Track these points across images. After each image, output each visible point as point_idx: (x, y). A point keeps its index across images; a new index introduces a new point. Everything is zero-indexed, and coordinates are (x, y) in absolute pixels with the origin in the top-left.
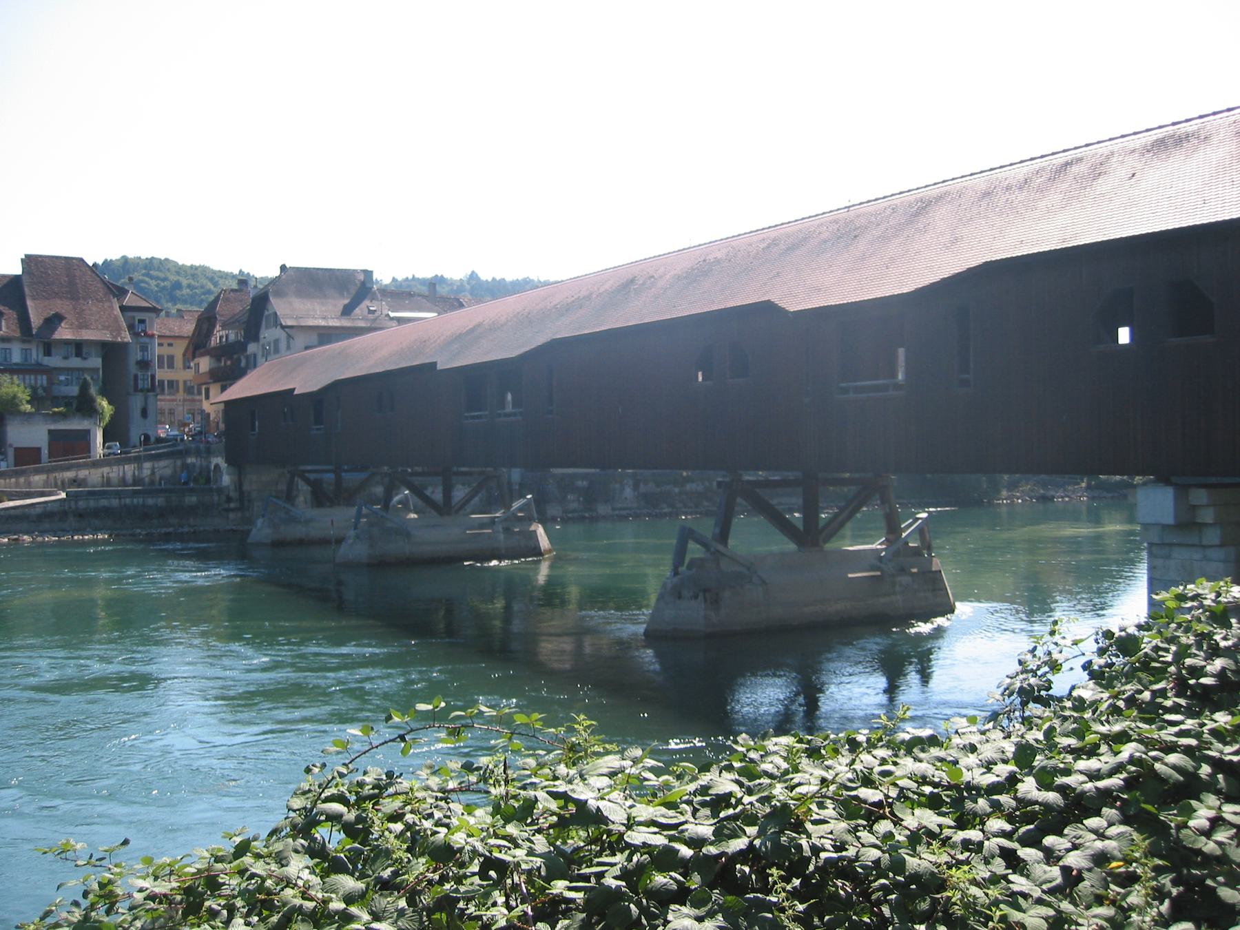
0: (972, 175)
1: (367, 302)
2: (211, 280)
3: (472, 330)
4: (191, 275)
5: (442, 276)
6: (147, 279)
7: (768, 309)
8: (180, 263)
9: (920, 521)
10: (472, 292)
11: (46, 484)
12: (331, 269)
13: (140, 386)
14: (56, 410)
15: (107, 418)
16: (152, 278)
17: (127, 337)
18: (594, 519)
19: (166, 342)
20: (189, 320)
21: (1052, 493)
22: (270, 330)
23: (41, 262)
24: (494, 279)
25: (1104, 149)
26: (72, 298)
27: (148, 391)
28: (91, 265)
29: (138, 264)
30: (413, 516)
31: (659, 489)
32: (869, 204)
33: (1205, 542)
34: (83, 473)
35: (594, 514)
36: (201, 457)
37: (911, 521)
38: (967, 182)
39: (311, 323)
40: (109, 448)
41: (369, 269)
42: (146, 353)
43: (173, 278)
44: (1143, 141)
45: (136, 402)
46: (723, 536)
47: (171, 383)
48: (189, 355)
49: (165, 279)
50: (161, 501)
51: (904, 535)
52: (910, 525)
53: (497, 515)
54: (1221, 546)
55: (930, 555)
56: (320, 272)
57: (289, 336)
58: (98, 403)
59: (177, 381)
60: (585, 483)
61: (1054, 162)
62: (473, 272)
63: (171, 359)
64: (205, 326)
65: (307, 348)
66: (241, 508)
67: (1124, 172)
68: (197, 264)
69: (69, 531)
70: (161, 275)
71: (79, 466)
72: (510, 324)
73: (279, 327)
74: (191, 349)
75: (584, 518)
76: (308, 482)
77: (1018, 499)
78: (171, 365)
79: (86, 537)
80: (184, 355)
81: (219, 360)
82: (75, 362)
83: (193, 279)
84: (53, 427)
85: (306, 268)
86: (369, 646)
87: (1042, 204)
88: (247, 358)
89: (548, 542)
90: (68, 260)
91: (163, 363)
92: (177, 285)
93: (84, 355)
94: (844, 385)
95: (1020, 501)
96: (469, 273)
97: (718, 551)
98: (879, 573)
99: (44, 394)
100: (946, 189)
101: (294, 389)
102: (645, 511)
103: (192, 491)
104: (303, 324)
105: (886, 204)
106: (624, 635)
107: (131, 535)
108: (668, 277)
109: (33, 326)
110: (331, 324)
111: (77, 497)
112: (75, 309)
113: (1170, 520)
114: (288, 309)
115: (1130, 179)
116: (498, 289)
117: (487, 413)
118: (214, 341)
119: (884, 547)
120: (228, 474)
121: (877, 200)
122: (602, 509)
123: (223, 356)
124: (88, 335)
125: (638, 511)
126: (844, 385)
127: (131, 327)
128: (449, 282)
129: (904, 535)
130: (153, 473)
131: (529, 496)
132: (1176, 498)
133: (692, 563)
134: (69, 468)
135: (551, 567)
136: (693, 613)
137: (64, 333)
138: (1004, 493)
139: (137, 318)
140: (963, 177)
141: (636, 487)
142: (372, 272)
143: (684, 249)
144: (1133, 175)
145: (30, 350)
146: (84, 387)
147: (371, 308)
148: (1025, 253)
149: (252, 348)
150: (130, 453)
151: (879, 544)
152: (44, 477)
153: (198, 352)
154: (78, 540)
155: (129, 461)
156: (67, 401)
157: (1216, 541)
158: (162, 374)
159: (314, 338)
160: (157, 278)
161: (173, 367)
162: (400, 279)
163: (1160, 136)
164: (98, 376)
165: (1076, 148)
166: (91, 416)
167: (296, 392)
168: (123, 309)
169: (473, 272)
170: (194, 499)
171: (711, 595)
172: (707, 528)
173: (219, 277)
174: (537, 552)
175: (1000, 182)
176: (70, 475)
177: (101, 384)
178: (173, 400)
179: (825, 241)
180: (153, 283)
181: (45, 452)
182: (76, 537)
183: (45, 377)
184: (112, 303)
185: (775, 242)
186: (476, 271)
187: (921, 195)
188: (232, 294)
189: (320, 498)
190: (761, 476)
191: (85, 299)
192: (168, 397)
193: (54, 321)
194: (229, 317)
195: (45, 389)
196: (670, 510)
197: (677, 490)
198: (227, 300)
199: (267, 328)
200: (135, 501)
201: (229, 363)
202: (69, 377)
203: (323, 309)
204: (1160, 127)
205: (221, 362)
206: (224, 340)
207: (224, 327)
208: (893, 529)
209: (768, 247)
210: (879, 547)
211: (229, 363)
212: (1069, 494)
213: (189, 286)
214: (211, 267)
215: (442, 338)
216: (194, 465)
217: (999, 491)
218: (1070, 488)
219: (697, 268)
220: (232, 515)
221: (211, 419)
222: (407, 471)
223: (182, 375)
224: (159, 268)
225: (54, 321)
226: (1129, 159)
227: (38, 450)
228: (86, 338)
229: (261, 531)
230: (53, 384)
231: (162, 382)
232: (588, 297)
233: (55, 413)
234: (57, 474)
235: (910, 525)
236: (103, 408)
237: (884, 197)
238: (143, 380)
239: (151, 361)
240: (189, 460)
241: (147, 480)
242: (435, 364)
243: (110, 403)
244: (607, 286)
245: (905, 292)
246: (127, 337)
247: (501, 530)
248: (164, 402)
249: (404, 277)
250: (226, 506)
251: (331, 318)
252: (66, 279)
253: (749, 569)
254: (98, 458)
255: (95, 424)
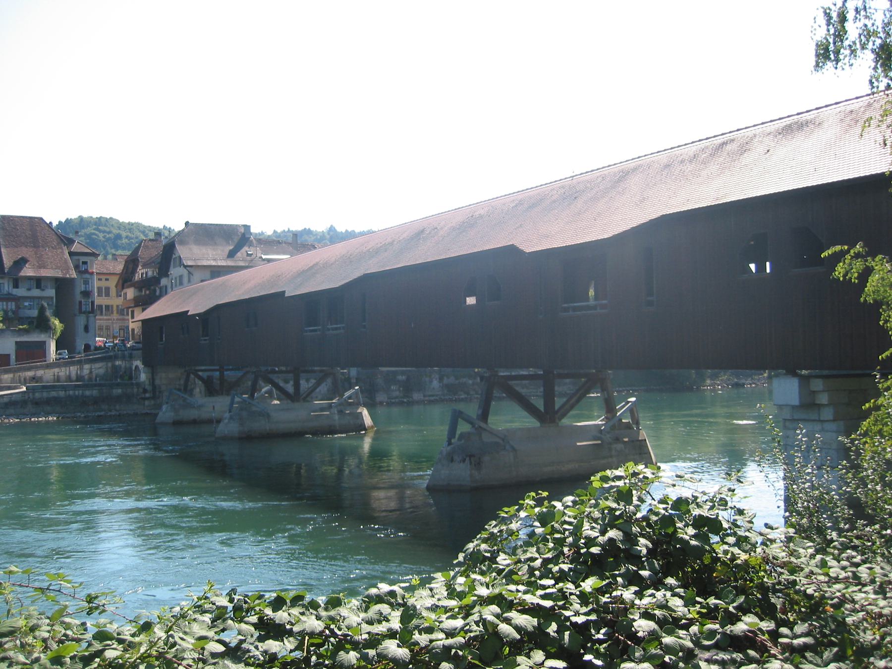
0: (658, 152)
1: (246, 248)
2: (143, 232)
3: (312, 267)
4: (129, 229)
5: (309, 229)
6: (97, 232)
7: (512, 250)
8: (121, 221)
9: (630, 404)
10: (331, 237)
11: (13, 380)
12: (220, 225)
13: (83, 309)
14: (21, 327)
15: (58, 334)
16: (100, 231)
17: (74, 274)
18: (410, 403)
19: (104, 277)
20: (121, 262)
21: (743, 381)
22: (176, 268)
23: (12, 220)
24: (275, 232)
25: (749, 133)
26: (34, 247)
27: (90, 313)
28: (48, 222)
29: (90, 222)
30: (276, 402)
31: (457, 382)
32: (587, 174)
33: (822, 419)
34: (40, 373)
35: (411, 400)
36: (126, 361)
37: (624, 403)
38: (655, 158)
39: (205, 263)
40: (60, 354)
41: (248, 224)
42: (87, 286)
43: (115, 231)
44: (777, 126)
45: (81, 321)
46: (484, 416)
47: (107, 307)
48: (120, 287)
49: (109, 232)
50: (95, 392)
51: (618, 414)
52: (623, 406)
53: (334, 401)
54: (834, 420)
55: (638, 428)
56: (213, 227)
57: (190, 273)
58: (51, 323)
59: (112, 306)
60: (404, 378)
61: (715, 142)
62: (332, 226)
63: (108, 289)
64: (131, 266)
65: (202, 281)
66: (154, 397)
67: (761, 149)
68: (133, 222)
69: (27, 415)
70: (107, 229)
71: (37, 368)
72: (337, 263)
73: (182, 267)
74: (121, 281)
75: (403, 402)
76: (200, 378)
77: (718, 386)
78: (108, 294)
79: (40, 419)
80: (116, 286)
81: (141, 290)
82: (36, 292)
83: (130, 232)
84: (18, 340)
85: (202, 224)
86: (225, 500)
87: (704, 173)
88: (161, 288)
89: (371, 420)
90: (31, 219)
91: (102, 294)
92: (118, 237)
93: (42, 288)
94: (566, 305)
95: (720, 387)
96: (329, 226)
97: (480, 427)
98: (600, 442)
99: (13, 316)
100: (640, 162)
101: (188, 311)
102: (447, 397)
103: (118, 385)
104: (200, 264)
105: (598, 174)
106: (238, 502)
107: (73, 417)
108: (446, 228)
109: (5, 266)
110: (219, 264)
111: (34, 390)
112: (36, 254)
113: (796, 402)
114: (188, 253)
115: (766, 153)
116: (349, 236)
117: (320, 327)
118: (137, 277)
119: (604, 422)
120: (144, 372)
121: (592, 171)
122: (416, 396)
123: (143, 287)
124: (44, 273)
125: (442, 397)
126: (566, 305)
127: (77, 267)
128: (314, 233)
129: (618, 414)
130: (91, 372)
131: (357, 388)
132: (800, 386)
133: (462, 436)
134: (29, 369)
135: (374, 439)
136: (462, 472)
137: (28, 271)
138: (708, 382)
139: (81, 260)
140: (652, 154)
141: (441, 379)
142: (249, 226)
143: (459, 208)
144: (768, 151)
145: (3, 283)
146: (42, 310)
147: (249, 253)
148: (690, 209)
149: (164, 281)
150: (75, 358)
151: (601, 421)
152: (11, 375)
153: (126, 285)
154: (35, 421)
155: (73, 363)
156: (29, 321)
157: (831, 418)
158: (98, 301)
159: (207, 274)
160: (104, 232)
161: (109, 296)
162: (279, 231)
163: (788, 123)
164: (53, 303)
165: (730, 132)
166: (46, 332)
167: (189, 314)
168: (71, 254)
169: (332, 226)
170: (120, 391)
171: (474, 458)
172: (472, 410)
173: (148, 230)
174: (362, 427)
175: (677, 157)
176: (30, 374)
177: (54, 308)
178: (109, 320)
179: (555, 201)
180: (101, 235)
181: (13, 357)
182: (33, 419)
183: (13, 303)
184: (63, 249)
185: (521, 203)
186: (334, 225)
187: (623, 167)
188: (150, 243)
189: (211, 390)
190: (532, 371)
191: (43, 247)
192: (105, 317)
193: (20, 263)
194: (148, 259)
195: (14, 312)
196: (466, 396)
197: (470, 382)
198: (146, 247)
199: (174, 267)
200: (77, 393)
201: (148, 292)
202: (32, 303)
203: (214, 253)
204: (789, 116)
205: (142, 292)
206: (144, 276)
207: (144, 266)
208: (610, 409)
209: (516, 206)
210: (600, 423)
211: (148, 292)
212: (756, 381)
213: (127, 237)
214: (143, 224)
215: (290, 275)
216: (120, 366)
217: (704, 380)
218: (756, 377)
219: (467, 222)
220: (147, 402)
221: (135, 332)
222: (275, 369)
223: (115, 301)
224: (105, 224)
225: (20, 263)
226: (766, 139)
227: (8, 356)
228: (44, 275)
229: (166, 414)
230: (20, 308)
231: (100, 307)
232: (392, 243)
233: (20, 329)
234: (21, 374)
235: (623, 406)
236: (55, 325)
237: (598, 169)
238: (86, 305)
239: (91, 292)
240: (117, 363)
241: (86, 377)
242: (284, 292)
243: (61, 322)
244: (405, 235)
245: (605, 237)
246: (74, 274)
247: (336, 412)
248: (101, 320)
249: (282, 230)
250: (143, 396)
251: (220, 260)
252: (30, 233)
253: (503, 440)
254: (52, 361)
255: (50, 337)
